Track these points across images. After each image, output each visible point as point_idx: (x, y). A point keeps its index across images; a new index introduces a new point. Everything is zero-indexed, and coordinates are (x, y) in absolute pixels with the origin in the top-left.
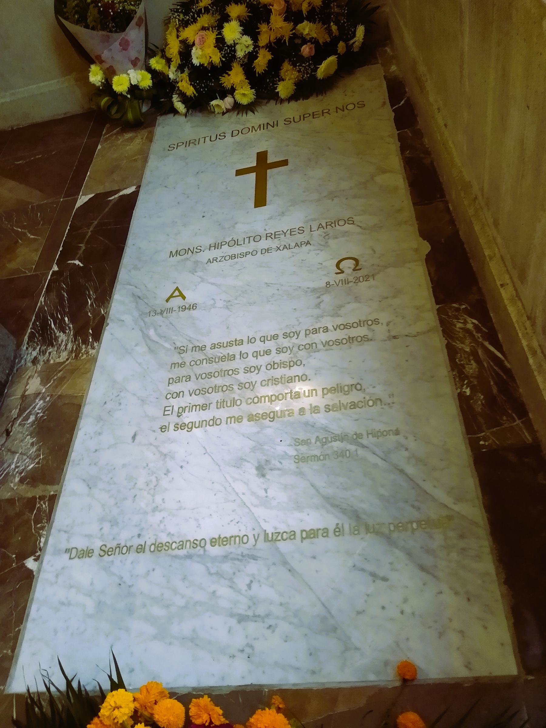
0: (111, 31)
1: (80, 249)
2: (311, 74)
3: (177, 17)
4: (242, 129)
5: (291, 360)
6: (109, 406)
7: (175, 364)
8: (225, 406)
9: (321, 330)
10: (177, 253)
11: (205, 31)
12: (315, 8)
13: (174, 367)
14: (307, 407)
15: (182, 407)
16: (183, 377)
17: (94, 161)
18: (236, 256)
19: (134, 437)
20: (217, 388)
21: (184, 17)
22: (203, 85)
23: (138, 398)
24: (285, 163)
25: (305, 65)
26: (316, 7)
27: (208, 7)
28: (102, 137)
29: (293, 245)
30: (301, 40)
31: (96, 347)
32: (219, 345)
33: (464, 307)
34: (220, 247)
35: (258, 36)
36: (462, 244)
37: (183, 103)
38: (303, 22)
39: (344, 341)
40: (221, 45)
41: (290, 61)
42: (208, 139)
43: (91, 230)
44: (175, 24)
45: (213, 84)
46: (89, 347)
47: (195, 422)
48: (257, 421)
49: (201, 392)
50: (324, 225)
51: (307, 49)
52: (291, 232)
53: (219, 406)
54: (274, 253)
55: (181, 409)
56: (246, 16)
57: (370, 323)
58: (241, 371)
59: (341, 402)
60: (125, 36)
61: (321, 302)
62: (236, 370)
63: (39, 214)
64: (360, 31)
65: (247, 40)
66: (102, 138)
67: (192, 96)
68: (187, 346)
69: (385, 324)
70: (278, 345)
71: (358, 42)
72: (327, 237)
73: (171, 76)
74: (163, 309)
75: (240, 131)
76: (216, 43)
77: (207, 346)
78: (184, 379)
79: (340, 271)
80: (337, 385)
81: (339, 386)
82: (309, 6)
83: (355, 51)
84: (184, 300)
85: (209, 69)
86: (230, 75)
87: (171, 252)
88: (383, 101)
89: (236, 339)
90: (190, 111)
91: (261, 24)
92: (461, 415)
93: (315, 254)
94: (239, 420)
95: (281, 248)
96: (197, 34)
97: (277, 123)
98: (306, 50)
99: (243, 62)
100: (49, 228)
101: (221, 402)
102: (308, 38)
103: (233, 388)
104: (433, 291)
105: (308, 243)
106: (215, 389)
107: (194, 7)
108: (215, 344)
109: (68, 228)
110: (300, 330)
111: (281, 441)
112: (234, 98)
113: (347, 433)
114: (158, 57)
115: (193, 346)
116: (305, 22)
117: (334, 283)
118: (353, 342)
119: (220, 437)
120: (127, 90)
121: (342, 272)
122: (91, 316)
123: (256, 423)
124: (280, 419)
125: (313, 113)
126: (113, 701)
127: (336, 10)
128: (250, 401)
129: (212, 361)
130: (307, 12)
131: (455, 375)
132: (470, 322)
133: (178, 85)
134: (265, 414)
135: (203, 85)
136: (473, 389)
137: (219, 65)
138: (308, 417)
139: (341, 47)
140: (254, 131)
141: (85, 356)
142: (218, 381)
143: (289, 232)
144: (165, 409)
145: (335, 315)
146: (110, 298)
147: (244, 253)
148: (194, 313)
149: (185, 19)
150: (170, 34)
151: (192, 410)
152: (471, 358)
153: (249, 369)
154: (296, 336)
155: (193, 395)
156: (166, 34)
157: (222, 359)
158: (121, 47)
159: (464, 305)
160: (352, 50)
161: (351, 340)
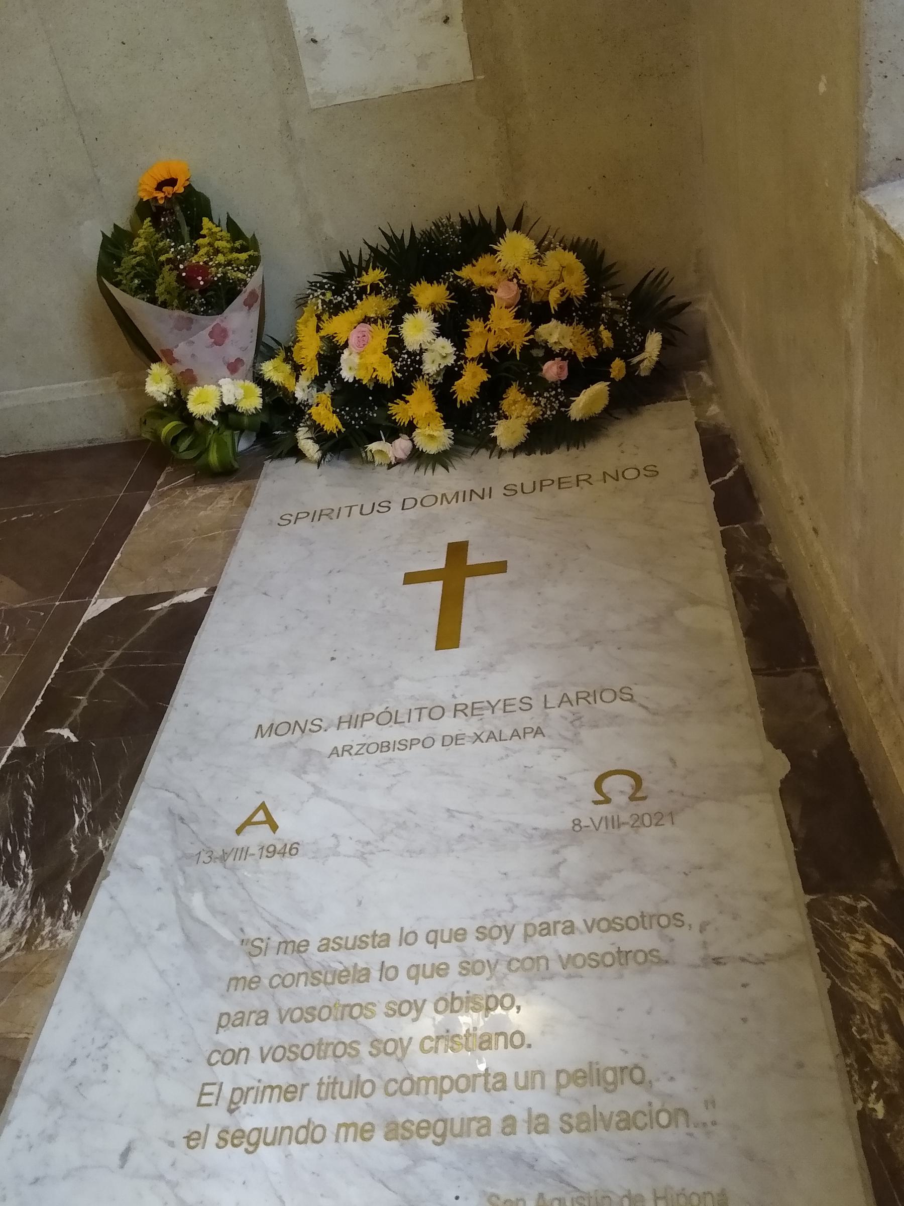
0: (196, 312)
1: (76, 707)
2: (558, 411)
3: (321, 297)
4: (424, 498)
5: (489, 994)
6: (79, 1071)
7: (237, 979)
8: (337, 1094)
9: (560, 927)
10: (271, 731)
11: (370, 324)
12: (572, 299)
13: (234, 988)
14: (521, 1116)
15: (240, 1089)
16: (251, 1013)
17: (132, 532)
18: (391, 746)
19: (125, 1155)
20: (323, 1047)
21: (332, 298)
22: (357, 415)
23: (148, 1058)
24: (500, 567)
25: (548, 395)
26: (575, 299)
27: (378, 284)
28: (155, 489)
29: (508, 732)
30: (544, 350)
31: (75, 925)
32: (337, 944)
33: (863, 904)
34: (359, 724)
35: (466, 339)
36: (855, 765)
37: (316, 442)
38: (549, 321)
39: (608, 960)
40: (396, 351)
41: (520, 385)
42: (356, 510)
43: (104, 668)
44: (315, 307)
45: (375, 415)
46: (60, 923)
47: (267, 1129)
48: (405, 1141)
49: (288, 1054)
50: (573, 697)
51: (555, 369)
52: (505, 705)
53: (323, 1095)
54: (468, 747)
55: (238, 1093)
56: (446, 304)
57: (664, 921)
58: (381, 1009)
59: (598, 1110)
60: (222, 321)
61: (560, 863)
62: (370, 1007)
63: (8, 628)
64: (654, 342)
65: (445, 346)
66: (154, 491)
67: (335, 432)
68: (269, 939)
69: (696, 928)
70: (464, 954)
71: (649, 360)
72: (577, 723)
73: (300, 395)
74: (228, 850)
75: (419, 501)
76: (387, 347)
77: (310, 944)
78: (253, 1017)
79: (602, 798)
80: (591, 1063)
81: (595, 1067)
82: (562, 296)
83: (643, 374)
84: (274, 833)
85: (371, 389)
86: (408, 402)
87: (260, 726)
88: (694, 467)
89: (375, 931)
90: (328, 456)
91: (472, 320)
92: (865, 1166)
93: (553, 756)
94: (364, 1133)
95: (484, 737)
96: (355, 328)
97: (490, 492)
98: (552, 370)
99: (435, 381)
100: (21, 658)
101: (328, 1083)
102: (557, 349)
103: (358, 1051)
104: (798, 861)
105: (539, 732)
106: (319, 1050)
107: (353, 282)
108: (328, 939)
109: (61, 660)
110: (514, 923)
111: (457, 1198)
112: (412, 440)
113: (611, 1192)
114: (279, 361)
115: (282, 941)
116: (554, 322)
117: (589, 823)
118: (627, 965)
119: (318, 1175)
120: (214, 413)
121: (607, 801)
122: (75, 851)
123: (402, 1145)
124: (459, 1141)
125: (559, 479)
126: (240, 837)
127: (610, 304)
128: (393, 1087)
129: (319, 980)
130: (558, 305)
131: (851, 1065)
132: (879, 941)
133: (309, 412)
134: (424, 1125)
135: (357, 415)
136: (890, 1102)
137: (389, 383)
138: (522, 1140)
139: (617, 368)
140: (445, 502)
141: (47, 944)
142: (327, 1030)
143: (501, 705)
144: (203, 1089)
145: (589, 896)
146: (121, 815)
147: (406, 741)
148: (291, 863)
149: (334, 302)
150: (306, 323)
151: (263, 1097)
152: (885, 1027)
153: (396, 1008)
154: (504, 937)
155: (269, 1060)
156: (298, 323)
157: (341, 977)
158: (213, 340)
159: (865, 900)
160: (636, 373)
161: (623, 956)
